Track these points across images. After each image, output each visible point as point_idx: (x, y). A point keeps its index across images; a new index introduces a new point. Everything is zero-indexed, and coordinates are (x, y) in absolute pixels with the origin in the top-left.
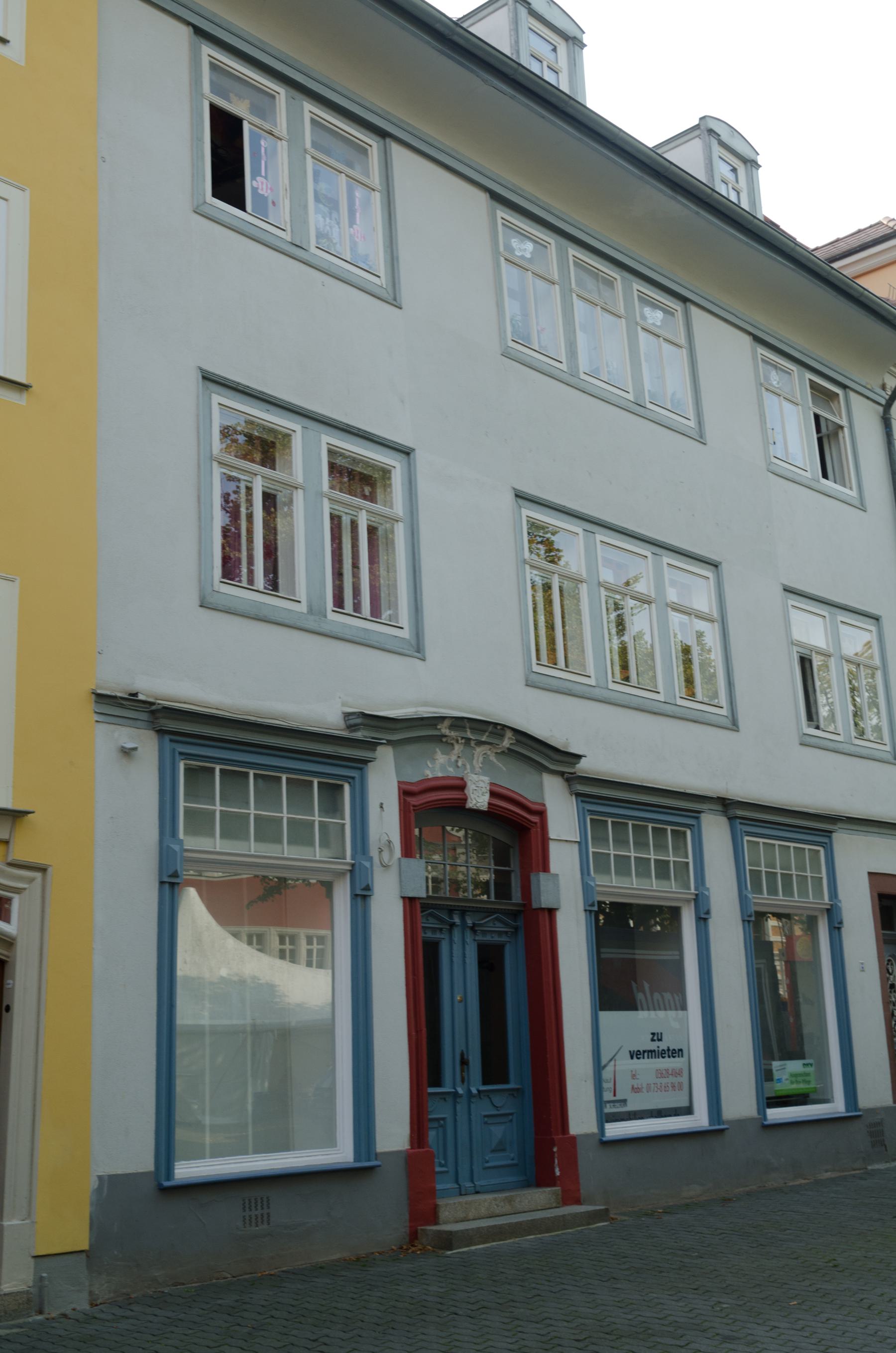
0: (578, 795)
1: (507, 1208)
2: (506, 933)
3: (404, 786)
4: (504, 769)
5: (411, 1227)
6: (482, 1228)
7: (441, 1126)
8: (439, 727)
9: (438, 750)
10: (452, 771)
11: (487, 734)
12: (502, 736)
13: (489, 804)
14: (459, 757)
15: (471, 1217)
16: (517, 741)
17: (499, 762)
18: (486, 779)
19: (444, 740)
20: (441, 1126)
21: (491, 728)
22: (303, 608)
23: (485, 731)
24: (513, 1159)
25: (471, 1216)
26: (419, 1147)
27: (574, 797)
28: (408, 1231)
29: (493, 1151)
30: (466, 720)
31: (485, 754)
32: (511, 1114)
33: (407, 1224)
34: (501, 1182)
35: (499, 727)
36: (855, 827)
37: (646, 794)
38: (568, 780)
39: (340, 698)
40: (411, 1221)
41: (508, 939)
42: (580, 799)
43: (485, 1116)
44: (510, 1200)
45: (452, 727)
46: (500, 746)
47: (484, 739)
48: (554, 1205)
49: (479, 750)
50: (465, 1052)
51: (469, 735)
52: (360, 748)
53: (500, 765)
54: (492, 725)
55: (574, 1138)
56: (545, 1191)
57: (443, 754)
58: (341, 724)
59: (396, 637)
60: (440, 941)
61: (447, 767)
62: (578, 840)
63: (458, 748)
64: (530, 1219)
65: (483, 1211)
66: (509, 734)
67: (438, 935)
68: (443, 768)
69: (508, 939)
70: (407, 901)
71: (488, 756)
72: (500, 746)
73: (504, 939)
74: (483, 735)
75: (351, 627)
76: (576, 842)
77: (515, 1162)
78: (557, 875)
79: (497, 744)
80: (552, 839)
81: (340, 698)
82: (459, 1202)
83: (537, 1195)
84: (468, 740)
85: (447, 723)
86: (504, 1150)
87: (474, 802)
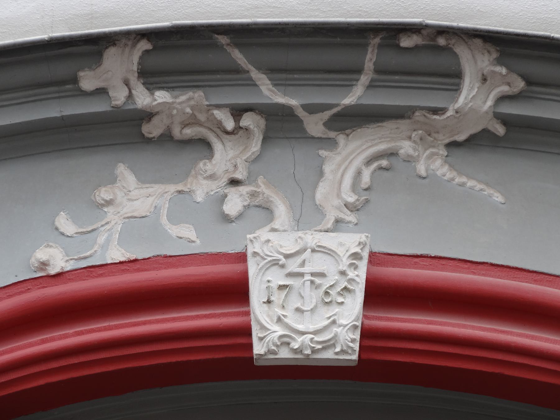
4: (498, 198)
9: (122, 169)
11: (364, 79)
14: (234, 182)
16: (529, 82)
18: (362, 237)
23: (359, 71)
30: (223, 40)
31: (392, 154)
35: (406, 42)
48: (95, 67)
57: (143, 180)
61: (164, 220)
72: (450, 113)
74: (349, 86)
79: (436, 111)
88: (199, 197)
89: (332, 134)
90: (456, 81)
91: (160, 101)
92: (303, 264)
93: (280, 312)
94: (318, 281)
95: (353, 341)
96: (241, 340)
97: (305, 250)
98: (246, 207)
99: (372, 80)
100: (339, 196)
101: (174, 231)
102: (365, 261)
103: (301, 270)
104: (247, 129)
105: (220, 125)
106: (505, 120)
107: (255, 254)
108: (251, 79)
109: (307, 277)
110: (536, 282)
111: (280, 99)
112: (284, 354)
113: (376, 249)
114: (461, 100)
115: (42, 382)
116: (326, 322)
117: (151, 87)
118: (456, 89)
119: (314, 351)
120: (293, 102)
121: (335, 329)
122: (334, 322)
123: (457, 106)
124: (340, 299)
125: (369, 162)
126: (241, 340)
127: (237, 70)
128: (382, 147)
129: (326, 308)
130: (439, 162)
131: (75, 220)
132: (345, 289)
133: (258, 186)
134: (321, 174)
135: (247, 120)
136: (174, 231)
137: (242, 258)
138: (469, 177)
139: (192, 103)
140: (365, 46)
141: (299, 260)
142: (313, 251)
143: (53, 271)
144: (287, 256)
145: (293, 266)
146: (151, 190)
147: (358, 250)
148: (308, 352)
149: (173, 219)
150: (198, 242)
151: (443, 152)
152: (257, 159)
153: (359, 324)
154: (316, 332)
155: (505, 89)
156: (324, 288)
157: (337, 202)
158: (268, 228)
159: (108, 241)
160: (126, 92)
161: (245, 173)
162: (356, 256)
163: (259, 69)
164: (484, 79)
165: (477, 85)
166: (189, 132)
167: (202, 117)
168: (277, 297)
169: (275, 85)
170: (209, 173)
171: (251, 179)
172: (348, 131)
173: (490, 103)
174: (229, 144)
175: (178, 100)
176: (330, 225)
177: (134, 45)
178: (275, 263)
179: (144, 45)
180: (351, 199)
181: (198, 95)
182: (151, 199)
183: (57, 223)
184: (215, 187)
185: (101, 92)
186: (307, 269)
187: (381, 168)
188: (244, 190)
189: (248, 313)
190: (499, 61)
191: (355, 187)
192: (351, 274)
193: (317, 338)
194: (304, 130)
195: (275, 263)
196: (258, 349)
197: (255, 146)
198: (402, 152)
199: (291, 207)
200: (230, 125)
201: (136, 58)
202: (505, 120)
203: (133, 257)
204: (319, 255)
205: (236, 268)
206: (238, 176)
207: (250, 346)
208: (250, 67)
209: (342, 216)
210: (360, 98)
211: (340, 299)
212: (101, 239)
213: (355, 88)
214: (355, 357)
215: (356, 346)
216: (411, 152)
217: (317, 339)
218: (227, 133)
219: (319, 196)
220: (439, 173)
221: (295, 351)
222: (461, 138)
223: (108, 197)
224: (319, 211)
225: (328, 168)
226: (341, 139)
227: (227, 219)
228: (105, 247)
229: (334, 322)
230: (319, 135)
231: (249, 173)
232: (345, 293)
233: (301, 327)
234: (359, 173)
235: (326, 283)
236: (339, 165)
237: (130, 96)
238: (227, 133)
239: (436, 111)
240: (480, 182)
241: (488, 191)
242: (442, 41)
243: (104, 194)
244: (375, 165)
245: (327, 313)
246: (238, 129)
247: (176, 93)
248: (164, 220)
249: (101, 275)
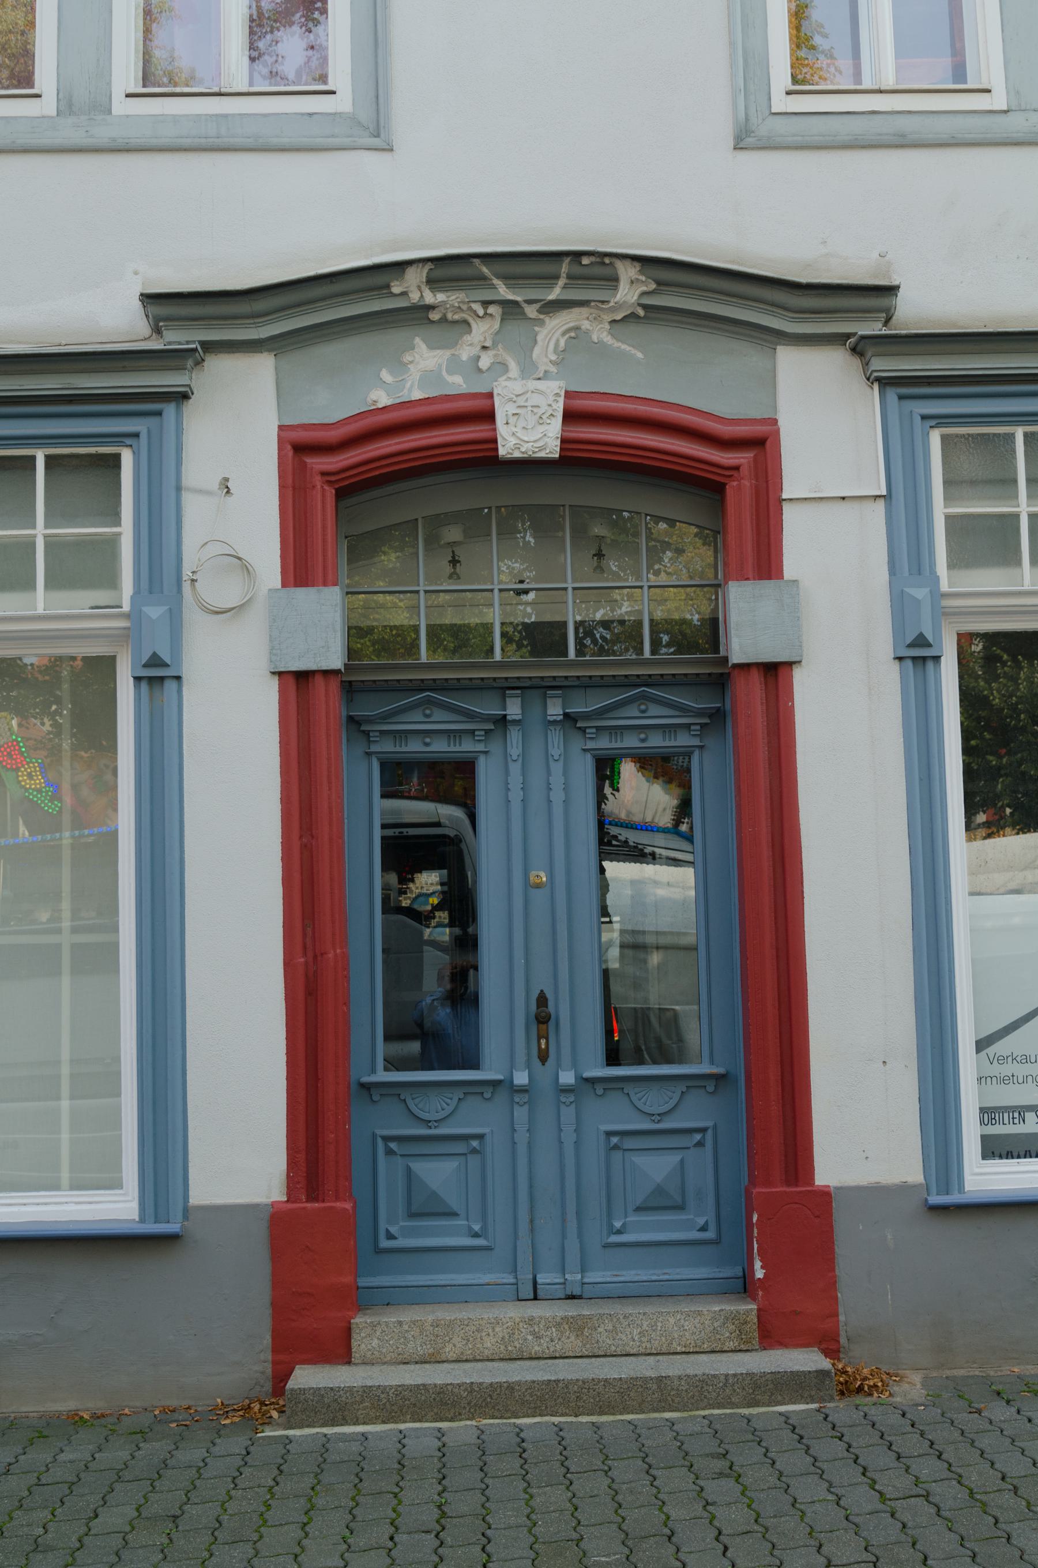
0: (885, 383)
1: (571, 1343)
2: (688, 726)
3: (295, 436)
4: (640, 355)
5: (274, 1363)
6: (383, 1389)
7: (474, 1151)
8: (396, 290)
9: (418, 340)
10: (457, 383)
11: (561, 282)
12: (613, 280)
13: (564, 441)
14: (484, 348)
15: (452, 1356)
16: (659, 283)
17: (618, 340)
18: (562, 383)
19: (434, 316)
20: (474, 1151)
21: (565, 267)
22: (47, 105)
23: (557, 277)
24: (703, 1229)
25: (449, 1351)
26: (310, 1199)
27: (876, 386)
28: (269, 1371)
29: (639, 1209)
30: (476, 261)
31: (577, 328)
32: (703, 1130)
33: (269, 1356)
34: (654, 1278)
35: (585, 261)
36: (684, 319)
37: (229, 352)
38: (856, 351)
39: (136, 273)
40: (275, 1350)
41: (696, 742)
42: (892, 394)
43: (609, 1134)
44: (578, 1326)
45: (432, 282)
46: (612, 304)
47: (555, 294)
48: (731, 1345)
49: (556, 325)
50: (549, 995)
51: (504, 292)
52: (124, 370)
53: (624, 347)
54: (567, 260)
55: (825, 1196)
56: (700, 1313)
57: (431, 347)
58: (143, 327)
59: (310, 115)
60: (476, 758)
61: (444, 373)
62: (884, 493)
63: (481, 331)
64: (488, 1380)
65: (489, 1344)
66: (627, 272)
67: (467, 746)
68: (429, 377)
69: (696, 742)
70: (291, 682)
71: (587, 332)
72: (612, 304)
73: (683, 740)
74: (551, 287)
75: (175, 119)
76: (876, 497)
77: (710, 1234)
78: (795, 582)
79: (603, 302)
80: (785, 500)
81: (136, 273)
82: (414, 1322)
83: (672, 1320)
84: (511, 308)
85: (414, 278)
86: (681, 1208)
87: (513, 441)
88: (464, 358)
89: (542, 316)
90: (614, 284)
91: (440, 300)
92: (527, 400)
93: (514, 429)
94: (535, 410)
95: (556, 446)
96: (491, 446)
97: (528, 392)
98: (493, 364)
99: (565, 284)
100: (546, 356)
101: (450, 379)
102: (562, 398)
103: (526, 404)
104: (491, 315)
105: (475, 312)
106: (645, 307)
107: (499, 394)
108: (493, 284)
109: (530, 408)
110: (662, 407)
111: (511, 297)
112: (517, 455)
113: (569, 389)
114: (618, 296)
115: (377, 473)
116: (541, 435)
117: (433, 290)
118: (616, 288)
119: (534, 452)
120: (519, 299)
121: (546, 440)
122: (545, 435)
123: (616, 300)
124: (549, 421)
125: (564, 334)
126: (491, 446)
127: (484, 278)
128: (572, 325)
129: (541, 426)
130: (605, 334)
131: (391, 373)
132: (552, 415)
133: (498, 350)
134: (535, 342)
135: (492, 309)
136: (450, 379)
137: (490, 395)
138: (623, 342)
139: (459, 300)
140: (562, 261)
141: (524, 398)
142: (532, 392)
143: (380, 406)
144: (517, 396)
145: (521, 401)
146: (435, 353)
147: (558, 391)
148: (531, 453)
149: (449, 372)
150: (465, 386)
151: (607, 326)
152: (497, 333)
153: (559, 436)
154: (534, 442)
155: (644, 289)
156: (539, 415)
157: (545, 360)
158: (505, 377)
159: (412, 386)
160: (419, 295)
161: (491, 342)
162: (557, 395)
163: (498, 278)
164: (632, 282)
165: (628, 286)
166: (456, 317)
167: (464, 307)
168: (513, 420)
169: (507, 288)
170: (469, 343)
171: (495, 344)
172: (551, 315)
173: (635, 298)
174: (480, 324)
175: (450, 299)
176: (541, 375)
177: (423, 266)
178: (510, 400)
179: (429, 266)
180: (554, 358)
181: (461, 296)
182: (436, 359)
183: (381, 376)
184: (476, 350)
185: (404, 294)
186: (529, 404)
187: (571, 337)
188: (491, 353)
189: (495, 430)
190: (641, 272)
191: (555, 351)
192: (555, 407)
193: (536, 445)
194: (524, 314)
195: (510, 400)
196: (502, 452)
197: (497, 325)
198: (583, 327)
199: (518, 363)
200: (481, 312)
201: (424, 275)
202: (645, 307)
203: (427, 396)
204: (536, 394)
205: (487, 402)
206: (487, 344)
207: (497, 449)
208: (493, 277)
209: (547, 368)
210: (558, 295)
211: (549, 421)
212: (408, 385)
213: (555, 289)
214: (557, 456)
215: (558, 449)
216: (588, 327)
217: (535, 445)
218: (479, 317)
219: (534, 356)
220: (605, 340)
221: (523, 453)
222: (619, 317)
223: (410, 359)
224: (534, 366)
225: (539, 338)
226: (547, 320)
227: (480, 370)
228: (410, 390)
229: (545, 435)
230: (534, 317)
231: (493, 342)
232: (551, 417)
233: (526, 439)
234: (558, 340)
235: (540, 411)
236: (547, 336)
237: (422, 296)
238: (479, 317)
239: (603, 302)
240: (629, 345)
241: (633, 351)
242: (607, 260)
243: (407, 358)
244: (567, 336)
245: (542, 428)
246: (486, 314)
247: (449, 294)
248: (444, 373)
249: (408, 408)
